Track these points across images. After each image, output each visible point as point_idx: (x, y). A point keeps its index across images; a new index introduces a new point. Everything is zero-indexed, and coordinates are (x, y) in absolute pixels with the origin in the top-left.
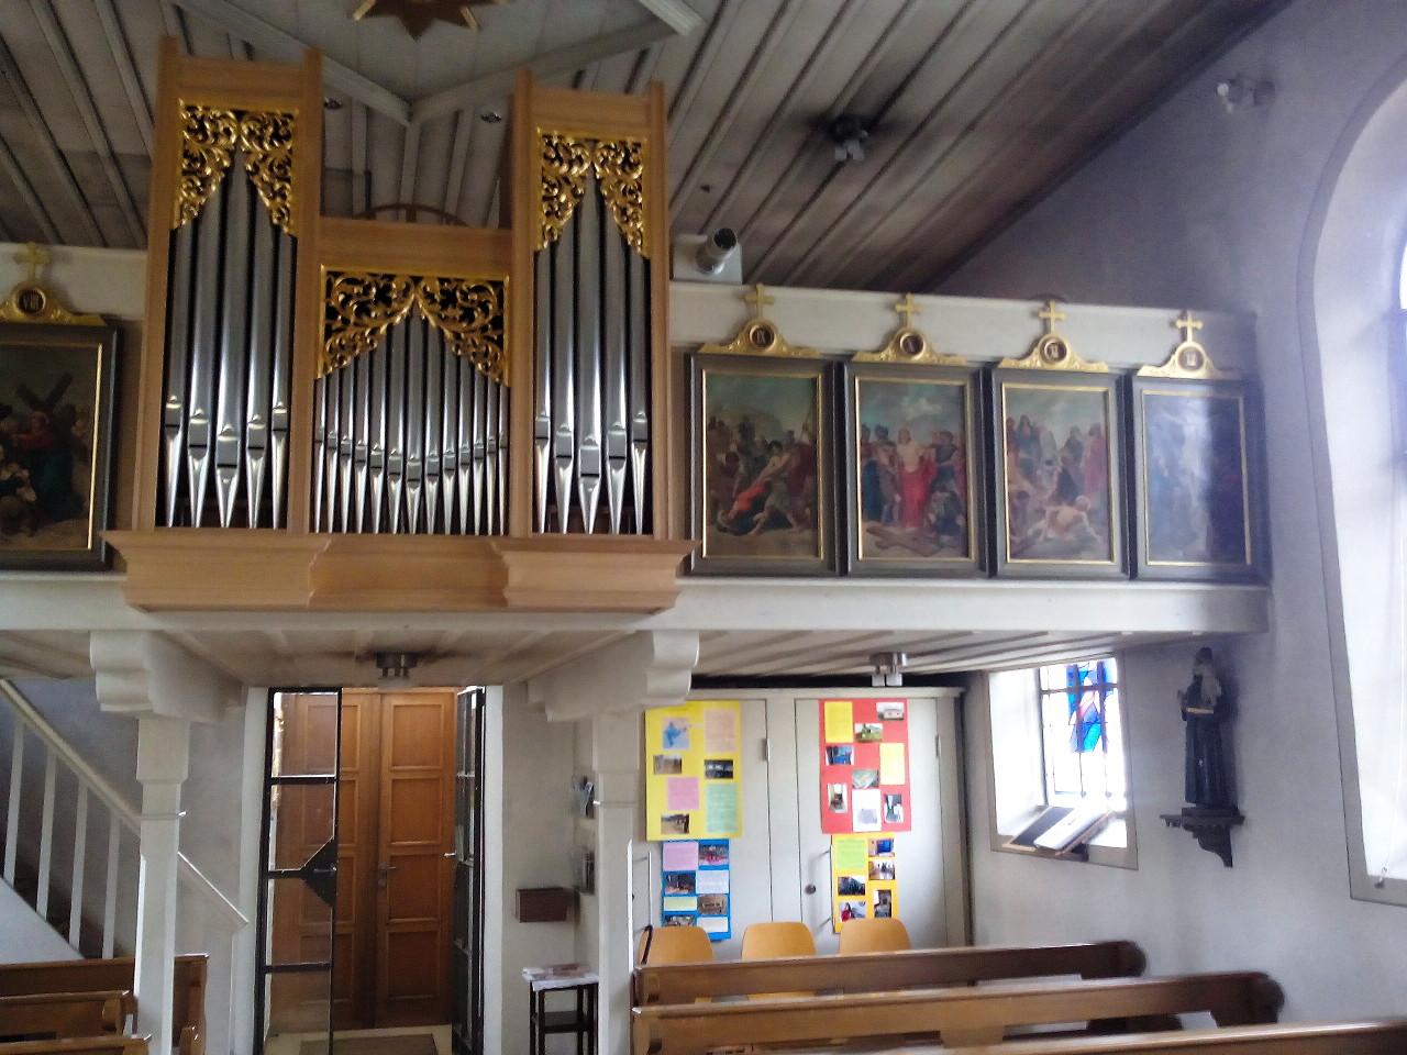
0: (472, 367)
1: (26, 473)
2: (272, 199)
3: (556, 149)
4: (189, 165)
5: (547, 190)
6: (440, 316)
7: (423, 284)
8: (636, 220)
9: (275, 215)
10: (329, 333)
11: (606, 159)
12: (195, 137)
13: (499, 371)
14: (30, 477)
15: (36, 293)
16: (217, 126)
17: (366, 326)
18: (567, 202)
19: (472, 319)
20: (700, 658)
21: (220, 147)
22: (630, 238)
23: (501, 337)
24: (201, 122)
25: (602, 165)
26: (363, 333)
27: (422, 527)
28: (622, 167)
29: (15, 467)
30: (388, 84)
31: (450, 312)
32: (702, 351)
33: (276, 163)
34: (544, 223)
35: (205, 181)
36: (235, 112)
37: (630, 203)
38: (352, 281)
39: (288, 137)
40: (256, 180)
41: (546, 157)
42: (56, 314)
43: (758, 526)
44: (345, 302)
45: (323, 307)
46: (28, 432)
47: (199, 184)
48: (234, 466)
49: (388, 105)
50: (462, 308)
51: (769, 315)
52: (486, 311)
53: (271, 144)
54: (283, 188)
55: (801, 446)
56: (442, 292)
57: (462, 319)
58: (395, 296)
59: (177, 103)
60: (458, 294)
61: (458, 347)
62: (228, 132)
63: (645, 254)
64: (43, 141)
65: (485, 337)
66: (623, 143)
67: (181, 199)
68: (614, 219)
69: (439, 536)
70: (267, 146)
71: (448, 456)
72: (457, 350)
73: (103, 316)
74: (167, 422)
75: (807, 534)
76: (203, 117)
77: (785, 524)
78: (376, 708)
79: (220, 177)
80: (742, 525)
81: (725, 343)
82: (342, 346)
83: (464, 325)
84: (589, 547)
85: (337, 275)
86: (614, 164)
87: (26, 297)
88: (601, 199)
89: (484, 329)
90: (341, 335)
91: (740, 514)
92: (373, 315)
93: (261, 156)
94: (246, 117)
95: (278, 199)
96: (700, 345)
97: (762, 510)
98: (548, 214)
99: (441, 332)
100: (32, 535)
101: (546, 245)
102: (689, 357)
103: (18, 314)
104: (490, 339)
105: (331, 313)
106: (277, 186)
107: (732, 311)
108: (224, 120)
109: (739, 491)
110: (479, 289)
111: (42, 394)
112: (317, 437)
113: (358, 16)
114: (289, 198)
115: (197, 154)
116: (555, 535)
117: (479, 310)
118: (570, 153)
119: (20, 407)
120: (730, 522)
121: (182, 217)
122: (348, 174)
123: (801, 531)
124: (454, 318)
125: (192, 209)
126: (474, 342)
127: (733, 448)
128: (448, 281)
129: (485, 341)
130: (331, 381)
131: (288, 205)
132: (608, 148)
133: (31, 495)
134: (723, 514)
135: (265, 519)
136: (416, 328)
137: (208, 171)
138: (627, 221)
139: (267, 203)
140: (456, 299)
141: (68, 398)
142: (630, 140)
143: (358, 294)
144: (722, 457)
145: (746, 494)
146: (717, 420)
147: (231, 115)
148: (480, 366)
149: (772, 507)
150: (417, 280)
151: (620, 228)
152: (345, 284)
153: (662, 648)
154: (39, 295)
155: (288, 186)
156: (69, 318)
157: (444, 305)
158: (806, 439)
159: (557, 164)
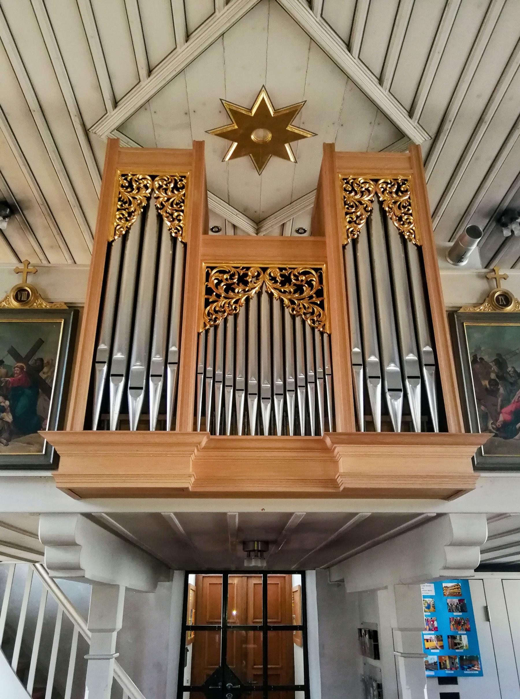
0: (303, 322)
1: (7, 403)
3: (352, 185)
4: (121, 205)
5: (348, 208)
6: (280, 291)
7: (268, 271)
8: (410, 223)
10: (207, 303)
13: (322, 324)
17: (232, 298)
18: (361, 215)
19: (302, 291)
20: (488, 537)
23: (322, 302)
24: (130, 183)
26: (229, 303)
28: (397, 193)
30: (245, 212)
31: (287, 288)
32: (461, 311)
33: (175, 202)
34: (348, 227)
36: (150, 176)
39: (183, 188)
41: (345, 190)
46: (12, 376)
47: (127, 215)
48: (142, 388)
49: (245, 225)
50: (295, 285)
52: (310, 284)
53: (172, 192)
56: (282, 276)
57: (295, 292)
59: (116, 172)
60: (292, 277)
61: (293, 310)
65: (311, 303)
67: (115, 224)
70: (170, 194)
72: (293, 311)
76: (131, 179)
78: (245, 584)
82: (216, 312)
85: (212, 268)
86: (391, 193)
87: (20, 293)
88: (383, 214)
90: (215, 304)
91: (505, 424)
92: (236, 291)
93: (166, 198)
98: (350, 222)
99: (282, 301)
100: (7, 445)
102: (453, 315)
103: (15, 304)
104: (316, 304)
105: (209, 291)
106: (176, 214)
109: (502, 407)
110: (305, 273)
111: (23, 353)
119: (9, 361)
120: (498, 429)
121: (115, 234)
124: (290, 292)
127: (493, 376)
128: (285, 269)
129: (312, 305)
135: (161, 425)
136: (265, 298)
139: (169, 224)
142: (400, 178)
143: (227, 279)
144: (486, 383)
146: (479, 357)
148: (309, 321)
153: (459, 528)
154: (27, 291)
156: (45, 305)
157: (283, 284)
159: (353, 194)
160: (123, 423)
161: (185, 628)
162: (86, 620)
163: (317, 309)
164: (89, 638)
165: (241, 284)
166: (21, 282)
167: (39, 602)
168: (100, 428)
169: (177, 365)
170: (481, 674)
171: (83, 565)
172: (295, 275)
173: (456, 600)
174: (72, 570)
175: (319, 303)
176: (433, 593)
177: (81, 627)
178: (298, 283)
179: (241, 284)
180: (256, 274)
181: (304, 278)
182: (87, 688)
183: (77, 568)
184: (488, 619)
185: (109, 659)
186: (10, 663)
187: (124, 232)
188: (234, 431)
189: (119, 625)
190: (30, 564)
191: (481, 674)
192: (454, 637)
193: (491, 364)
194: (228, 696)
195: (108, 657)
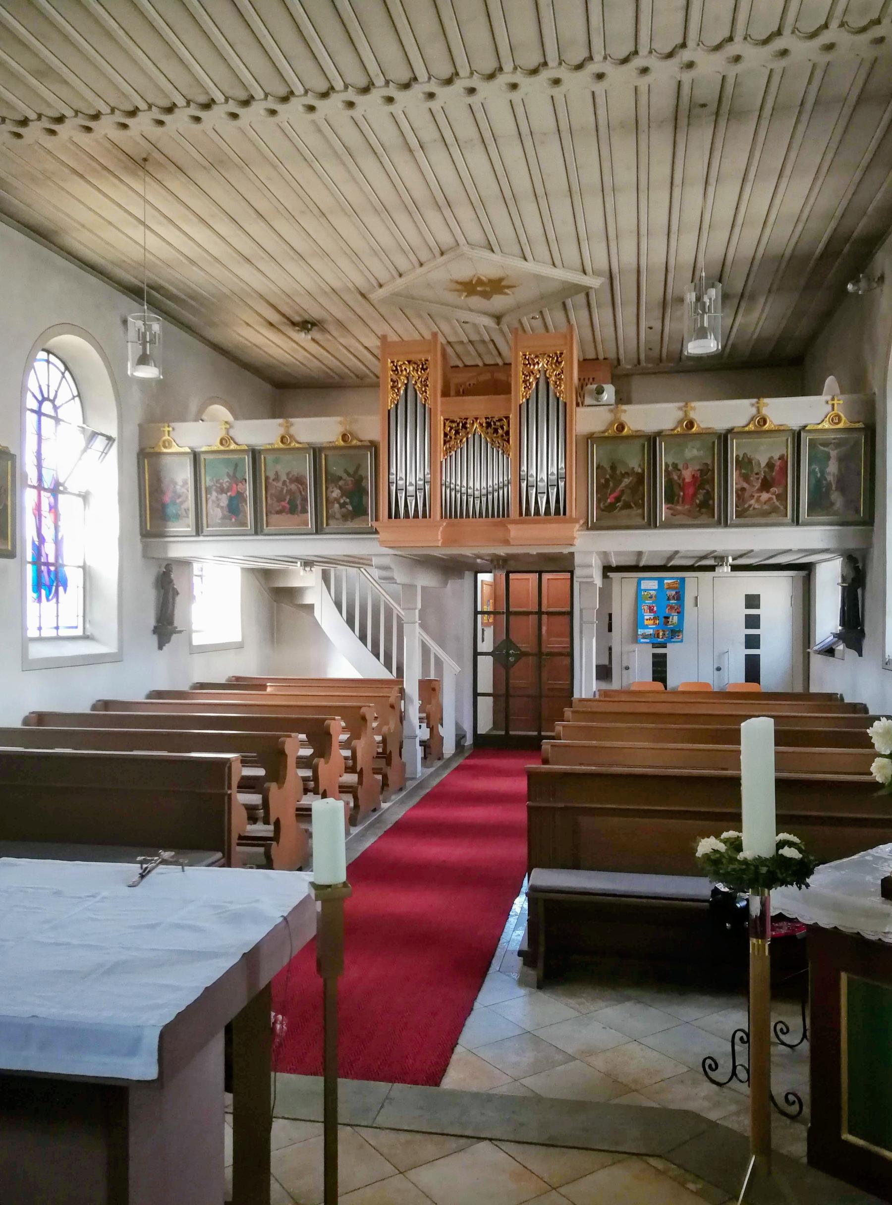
10: (445, 443)
19: (497, 432)
85: (447, 420)
105: (446, 435)
110: (500, 420)
111: (351, 471)
127: (608, 476)
136: (477, 437)
144: (603, 481)
160: (407, 515)
162: (399, 605)
168: (395, 518)
170: (682, 641)
173: (673, 593)
174: (391, 579)
176: (656, 587)
177: (398, 609)
183: (393, 579)
184: (697, 605)
186: (354, 631)
188: (461, 516)
189: (419, 606)
191: (682, 641)
192: (667, 618)
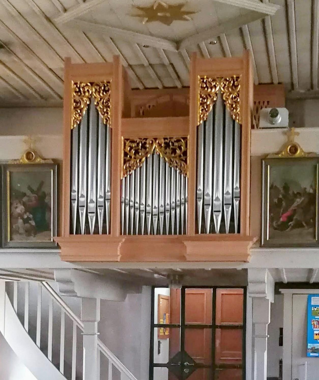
2: (103, 115)
3: (206, 83)
4: (76, 105)
9: (105, 121)
10: (125, 162)
11: (225, 85)
12: (77, 95)
14: (33, 217)
15: (31, 153)
16: (85, 89)
21: (86, 97)
22: (234, 117)
24: (79, 88)
25: (224, 88)
26: (136, 162)
27: (158, 232)
29: (28, 214)
31: (168, 150)
32: (269, 157)
35: (81, 110)
36: (90, 83)
37: (234, 102)
38: (133, 142)
39: (108, 91)
40: (98, 108)
42: (38, 160)
43: (290, 227)
44: (130, 150)
45: (123, 152)
46: (31, 201)
51: (297, 140)
53: (103, 94)
54: (107, 110)
55: (310, 194)
56: (165, 143)
58: (148, 146)
60: (170, 144)
62: (88, 91)
63: (240, 123)
64: (42, 66)
66: (232, 78)
68: (228, 109)
69: (170, 235)
71: (178, 203)
73: (53, 160)
74: (72, 198)
75: (311, 230)
77: (302, 226)
79: (86, 109)
80: (283, 227)
81: (277, 153)
83: (173, 155)
84: (220, 239)
85: (127, 140)
89: (180, 156)
91: (283, 222)
94: (94, 85)
95: (106, 115)
96: (267, 155)
97: (292, 221)
100: (35, 237)
101: (201, 122)
105: (126, 154)
107: (282, 139)
108: (86, 87)
109: (282, 214)
110: (178, 141)
111: (35, 188)
112: (122, 201)
113: (144, 23)
114: (109, 114)
115: (78, 101)
116: (197, 235)
117: (178, 149)
118: (212, 84)
119: (28, 193)
120: (278, 226)
121: (74, 124)
122: (163, 65)
123: (308, 229)
125: (77, 121)
126: (176, 162)
127: (281, 196)
130: (131, 177)
131: (109, 116)
132: (226, 80)
133: (33, 223)
134: (276, 223)
135: (104, 232)
137: (82, 106)
138: (233, 110)
139: (102, 117)
140: (170, 145)
141: (44, 189)
144: (276, 200)
145: (285, 215)
146: (274, 185)
147: (89, 84)
149: (296, 219)
150: (156, 139)
151: (230, 113)
152: (130, 143)
154: (32, 154)
155: (109, 109)
156: (43, 161)
158: (311, 191)
159: (206, 89)
161: (153, 326)
163: (183, 163)
164: (83, 328)
165: (143, 149)
166: (28, 148)
167: (48, 306)
169: (110, 200)
171: (76, 291)
172: (172, 142)
174: (71, 293)
175: (184, 160)
177: (78, 321)
178: (174, 147)
179: (143, 149)
180: (151, 142)
181: (177, 144)
182: (84, 348)
183: (74, 292)
185: (94, 335)
186: (35, 342)
187: (79, 123)
188: (140, 233)
190: (39, 282)
193: (280, 189)
194: (186, 370)
195: (94, 334)
